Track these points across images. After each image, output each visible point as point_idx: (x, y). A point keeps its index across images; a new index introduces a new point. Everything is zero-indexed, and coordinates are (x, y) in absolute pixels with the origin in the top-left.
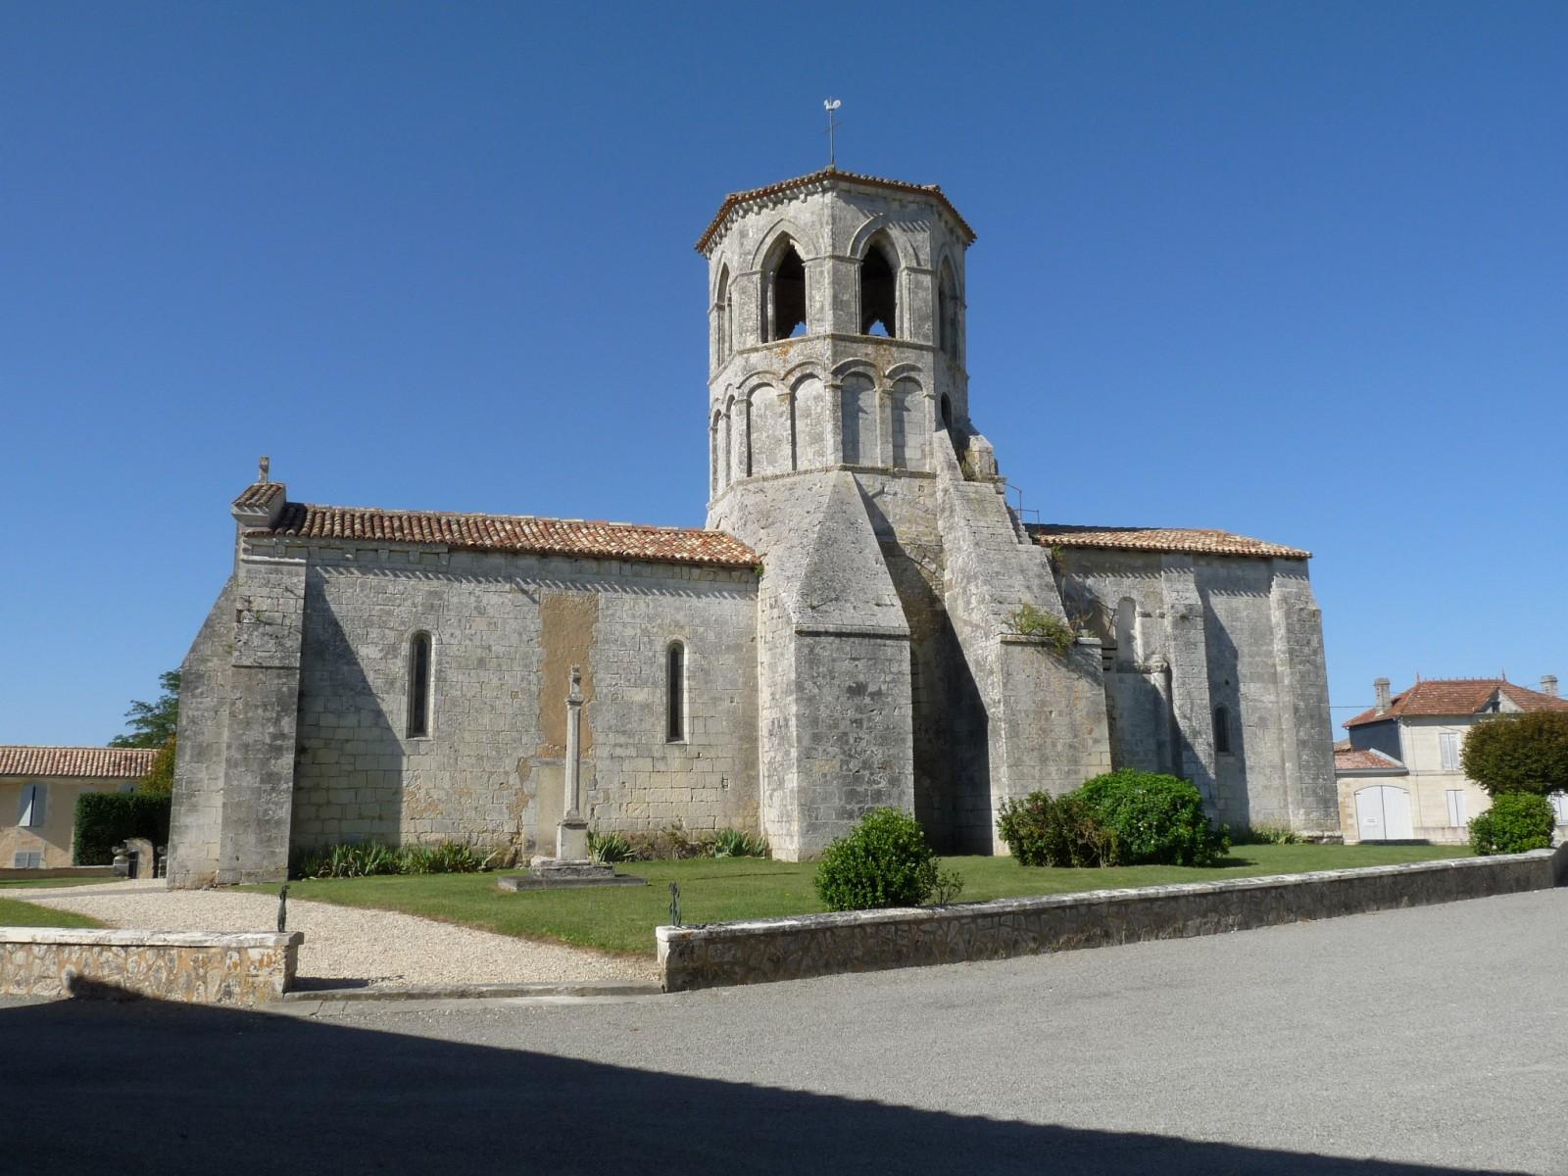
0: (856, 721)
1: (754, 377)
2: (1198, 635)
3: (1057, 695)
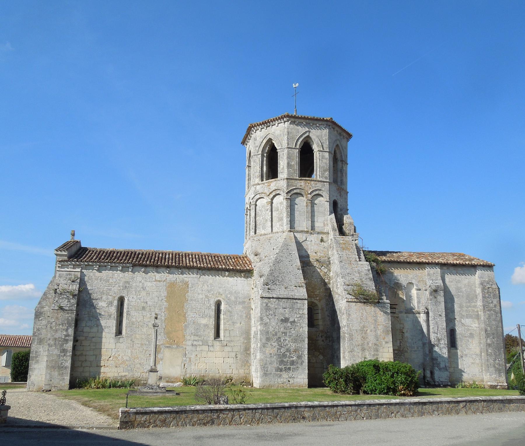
2: (441, 298)
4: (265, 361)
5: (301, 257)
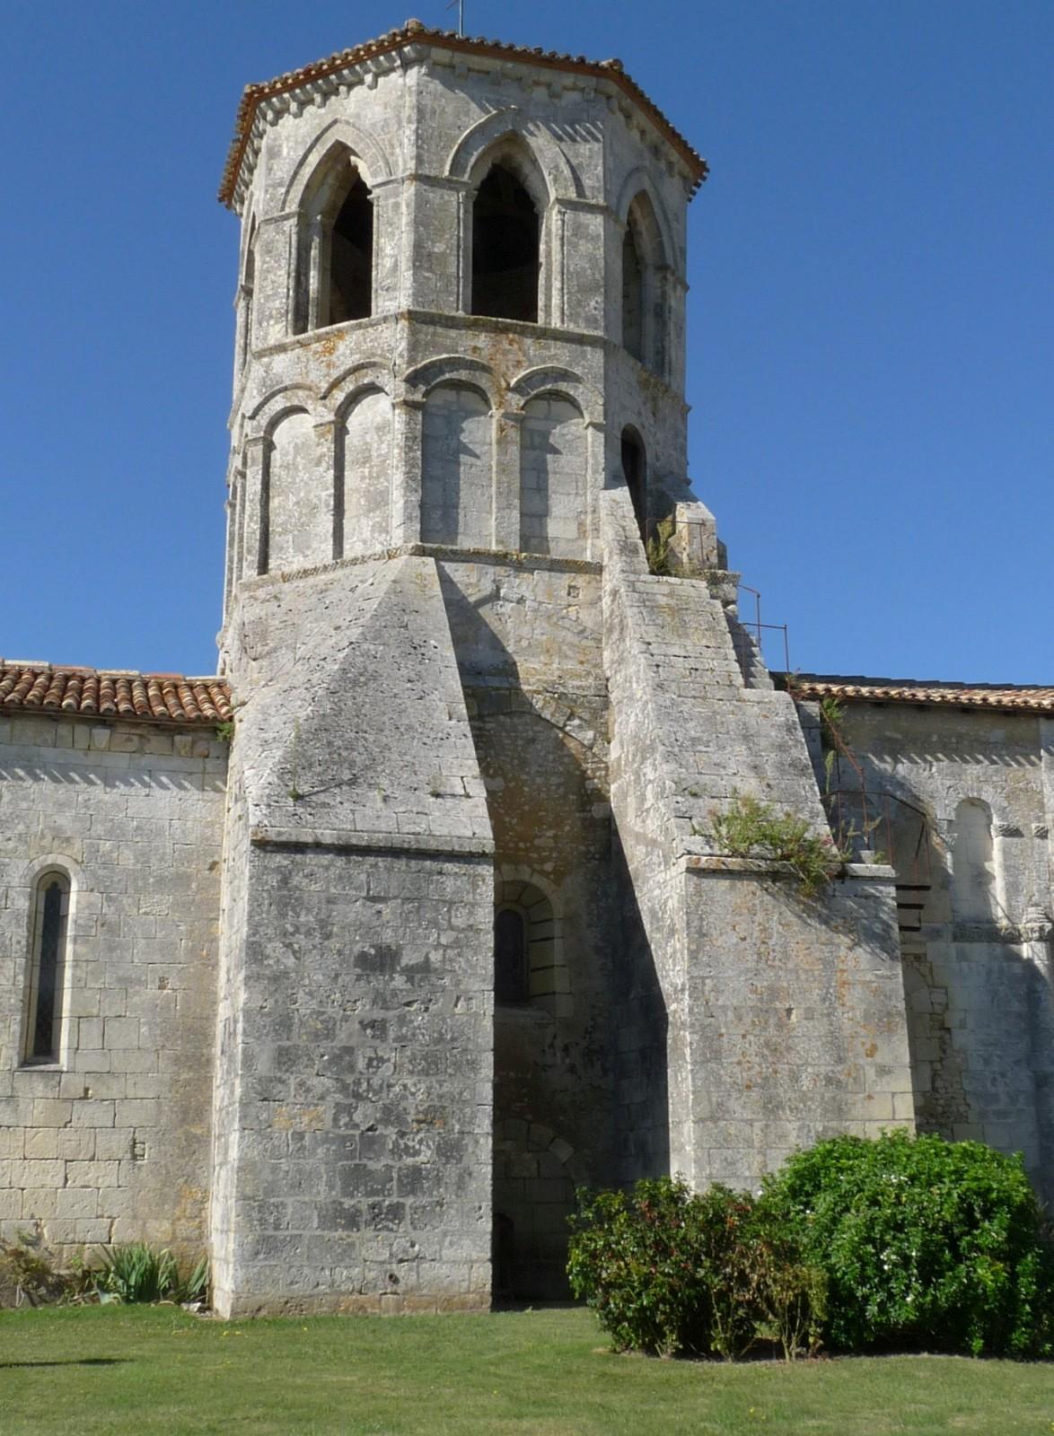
0: (372, 1024)
1: (278, 398)
3: (803, 977)
4: (267, 1175)
5: (468, 671)
